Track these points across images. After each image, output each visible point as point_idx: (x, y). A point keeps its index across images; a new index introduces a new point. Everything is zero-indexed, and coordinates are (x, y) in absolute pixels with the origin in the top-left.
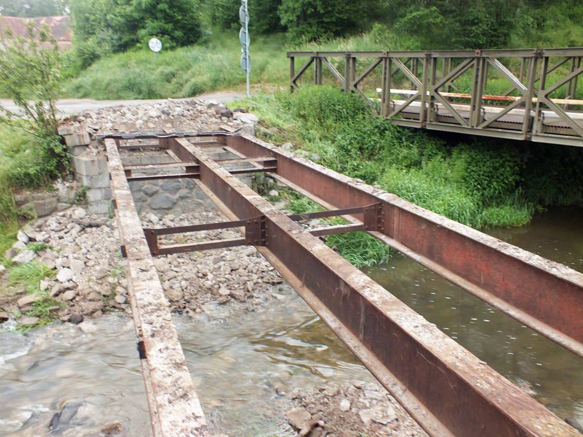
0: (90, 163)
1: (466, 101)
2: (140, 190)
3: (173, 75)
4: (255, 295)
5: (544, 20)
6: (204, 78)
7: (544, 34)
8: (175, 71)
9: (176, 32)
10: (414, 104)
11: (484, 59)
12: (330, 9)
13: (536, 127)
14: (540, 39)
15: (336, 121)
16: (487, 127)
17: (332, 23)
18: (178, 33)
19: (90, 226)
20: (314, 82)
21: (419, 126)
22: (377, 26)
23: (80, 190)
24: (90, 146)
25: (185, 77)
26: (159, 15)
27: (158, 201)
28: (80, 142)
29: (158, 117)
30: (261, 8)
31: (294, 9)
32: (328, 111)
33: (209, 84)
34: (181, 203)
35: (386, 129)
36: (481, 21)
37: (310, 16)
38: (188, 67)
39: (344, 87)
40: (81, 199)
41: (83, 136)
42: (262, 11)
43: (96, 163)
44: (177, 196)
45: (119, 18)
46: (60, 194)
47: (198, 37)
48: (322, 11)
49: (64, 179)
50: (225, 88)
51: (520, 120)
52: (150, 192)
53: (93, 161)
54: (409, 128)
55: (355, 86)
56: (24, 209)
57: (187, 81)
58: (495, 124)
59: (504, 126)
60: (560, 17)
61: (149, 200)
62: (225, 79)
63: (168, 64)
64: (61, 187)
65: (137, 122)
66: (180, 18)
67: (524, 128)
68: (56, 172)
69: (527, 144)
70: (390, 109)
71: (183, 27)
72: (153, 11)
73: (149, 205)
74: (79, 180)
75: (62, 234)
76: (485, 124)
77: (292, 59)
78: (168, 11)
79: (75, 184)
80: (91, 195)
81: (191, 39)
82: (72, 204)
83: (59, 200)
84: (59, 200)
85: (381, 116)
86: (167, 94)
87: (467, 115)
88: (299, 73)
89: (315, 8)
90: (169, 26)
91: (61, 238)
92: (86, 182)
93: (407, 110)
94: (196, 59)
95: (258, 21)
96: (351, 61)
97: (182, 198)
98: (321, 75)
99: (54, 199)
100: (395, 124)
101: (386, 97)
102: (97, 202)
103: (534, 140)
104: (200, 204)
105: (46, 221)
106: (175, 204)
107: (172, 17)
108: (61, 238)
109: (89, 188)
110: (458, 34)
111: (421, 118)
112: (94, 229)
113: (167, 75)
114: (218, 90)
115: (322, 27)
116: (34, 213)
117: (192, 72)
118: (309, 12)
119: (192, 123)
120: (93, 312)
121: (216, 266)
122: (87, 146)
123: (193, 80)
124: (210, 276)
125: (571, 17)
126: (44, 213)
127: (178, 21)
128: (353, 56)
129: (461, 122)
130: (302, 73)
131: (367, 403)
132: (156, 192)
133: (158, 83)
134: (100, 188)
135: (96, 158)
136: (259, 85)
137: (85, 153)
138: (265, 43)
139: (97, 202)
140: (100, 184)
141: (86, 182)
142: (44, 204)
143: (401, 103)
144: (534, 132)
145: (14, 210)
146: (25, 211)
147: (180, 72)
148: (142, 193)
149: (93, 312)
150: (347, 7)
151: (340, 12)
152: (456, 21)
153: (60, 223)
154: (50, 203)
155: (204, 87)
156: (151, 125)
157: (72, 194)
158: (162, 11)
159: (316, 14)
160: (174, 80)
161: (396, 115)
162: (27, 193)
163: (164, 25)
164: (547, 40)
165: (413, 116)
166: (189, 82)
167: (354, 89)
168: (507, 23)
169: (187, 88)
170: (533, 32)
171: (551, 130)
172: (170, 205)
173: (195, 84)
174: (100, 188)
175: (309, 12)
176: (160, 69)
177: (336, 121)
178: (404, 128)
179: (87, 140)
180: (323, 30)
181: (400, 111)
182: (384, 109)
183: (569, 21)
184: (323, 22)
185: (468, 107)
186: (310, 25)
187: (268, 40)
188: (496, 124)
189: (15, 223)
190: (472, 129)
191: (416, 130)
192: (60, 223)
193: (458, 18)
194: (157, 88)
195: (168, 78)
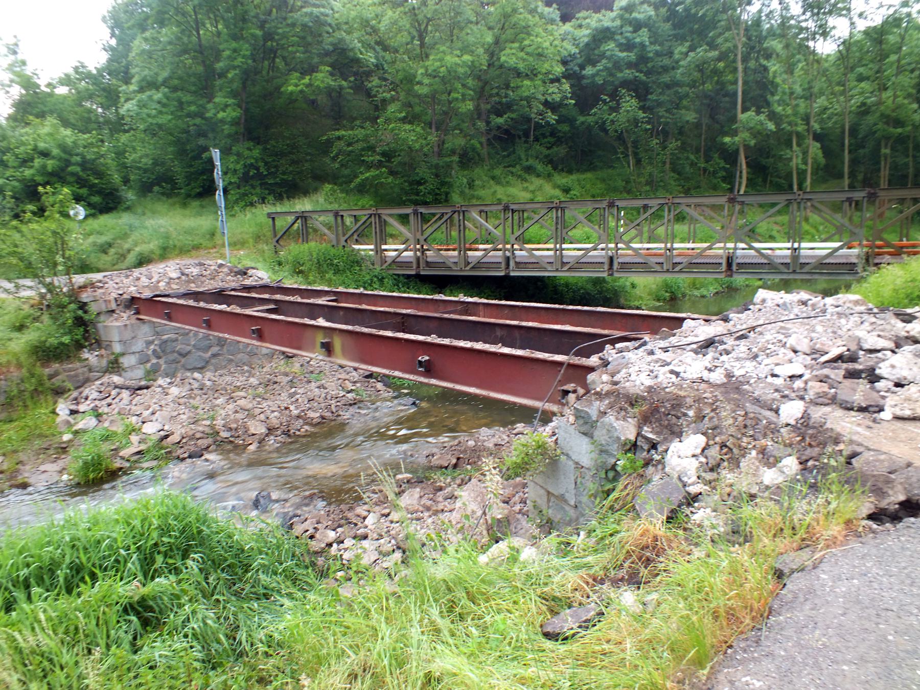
0: (123, 328)
1: (454, 250)
2: (174, 352)
3: (110, 245)
4: (341, 413)
5: (473, 181)
6: (153, 246)
7: (476, 193)
8: (112, 241)
9: (93, 198)
10: (405, 254)
11: (464, 212)
12: (273, 170)
13: (512, 264)
14: (473, 197)
15: (335, 274)
16: (473, 268)
17: (276, 184)
18: (96, 199)
19: (140, 388)
20: (301, 240)
21: (413, 273)
22: (328, 187)
23: (112, 357)
24: (117, 312)
25: (126, 246)
26: (72, 179)
27: (192, 360)
28: (107, 307)
29: (179, 278)
30: (192, 170)
31: (235, 171)
32: (325, 266)
33: (158, 252)
34: (213, 361)
35: (383, 278)
36: (426, 182)
37: (252, 177)
38: (125, 236)
39: (334, 243)
40: (114, 366)
41: (110, 301)
42: (192, 173)
43: (129, 327)
44: (210, 353)
45: (16, 184)
46: (91, 363)
47: (119, 203)
48: (265, 173)
49: (91, 349)
50: (177, 255)
51: (499, 260)
52: (184, 352)
53: (126, 325)
54: (403, 275)
55: (346, 241)
56: (57, 381)
57: (129, 251)
58: (478, 265)
59: (485, 266)
60: (485, 178)
61: (183, 360)
62: (175, 246)
63: (100, 233)
64: (90, 357)
65: (160, 284)
66: (96, 181)
67: (503, 266)
68: (82, 341)
69: (507, 277)
70: (383, 260)
71: (100, 192)
72: (62, 175)
73: (183, 366)
74: (108, 347)
75: (109, 400)
76: (471, 266)
77: (273, 219)
78: (81, 173)
79: (103, 352)
80: (126, 361)
81: (111, 205)
82: (105, 372)
83: (90, 370)
84: (90, 370)
85: (376, 266)
86: (106, 266)
87: (456, 260)
88: (281, 233)
89: (257, 169)
90: (84, 191)
91: (109, 405)
92: (117, 348)
93: (398, 260)
94: (131, 227)
95: (188, 185)
96: (339, 219)
97: (214, 355)
98: (305, 235)
99: (85, 369)
100: (391, 272)
101: (379, 251)
102: (132, 368)
103: (512, 274)
104: (231, 361)
105: (81, 393)
106: (207, 362)
107: (86, 181)
108: (109, 405)
109: (123, 354)
110: (407, 194)
111: (415, 266)
112: (145, 391)
113: (102, 246)
114: (169, 258)
115: (266, 189)
116: (69, 385)
117: (133, 240)
118: (251, 173)
119: (212, 282)
120: (208, 447)
121: (293, 399)
122: (113, 311)
123: (138, 249)
124: (292, 407)
125: (493, 178)
126: (79, 384)
127: (94, 185)
128: (341, 213)
129: (452, 265)
130: (285, 233)
131: (486, 438)
132: (189, 352)
133: (93, 255)
134: (133, 353)
135: (128, 322)
136: (215, 250)
137: (112, 319)
138: (202, 207)
139: (132, 368)
140: (135, 348)
141: (117, 348)
142: (76, 376)
143: (394, 254)
144: (511, 268)
145: (48, 384)
146: (58, 384)
147: (119, 241)
148: (176, 355)
149: (208, 447)
150: (291, 169)
151: (284, 173)
152: (405, 181)
153: (101, 392)
154: (83, 374)
155: (153, 256)
156: (174, 286)
157: (104, 362)
158: (73, 174)
159: (259, 176)
160: (112, 251)
161: (390, 265)
162: (56, 366)
163: (78, 190)
164: (479, 198)
165: (407, 265)
166: (132, 252)
167: (345, 244)
168: (446, 183)
169: (131, 258)
170: (467, 191)
171: (522, 266)
172: (203, 364)
173: (140, 254)
174: (133, 353)
175: (251, 173)
176: (91, 239)
177: (335, 274)
178: (398, 275)
179: (113, 306)
180: (267, 192)
181: (393, 262)
182: (377, 260)
183: (492, 182)
184: (266, 183)
185: (456, 253)
186: (253, 187)
187: (204, 203)
188: (479, 265)
189: (49, 398)
190: (461, 270)
191: (408, 277)
192: (101, 392)
193: (406, 178)
194: (93, 260)
195: (104, 249)
